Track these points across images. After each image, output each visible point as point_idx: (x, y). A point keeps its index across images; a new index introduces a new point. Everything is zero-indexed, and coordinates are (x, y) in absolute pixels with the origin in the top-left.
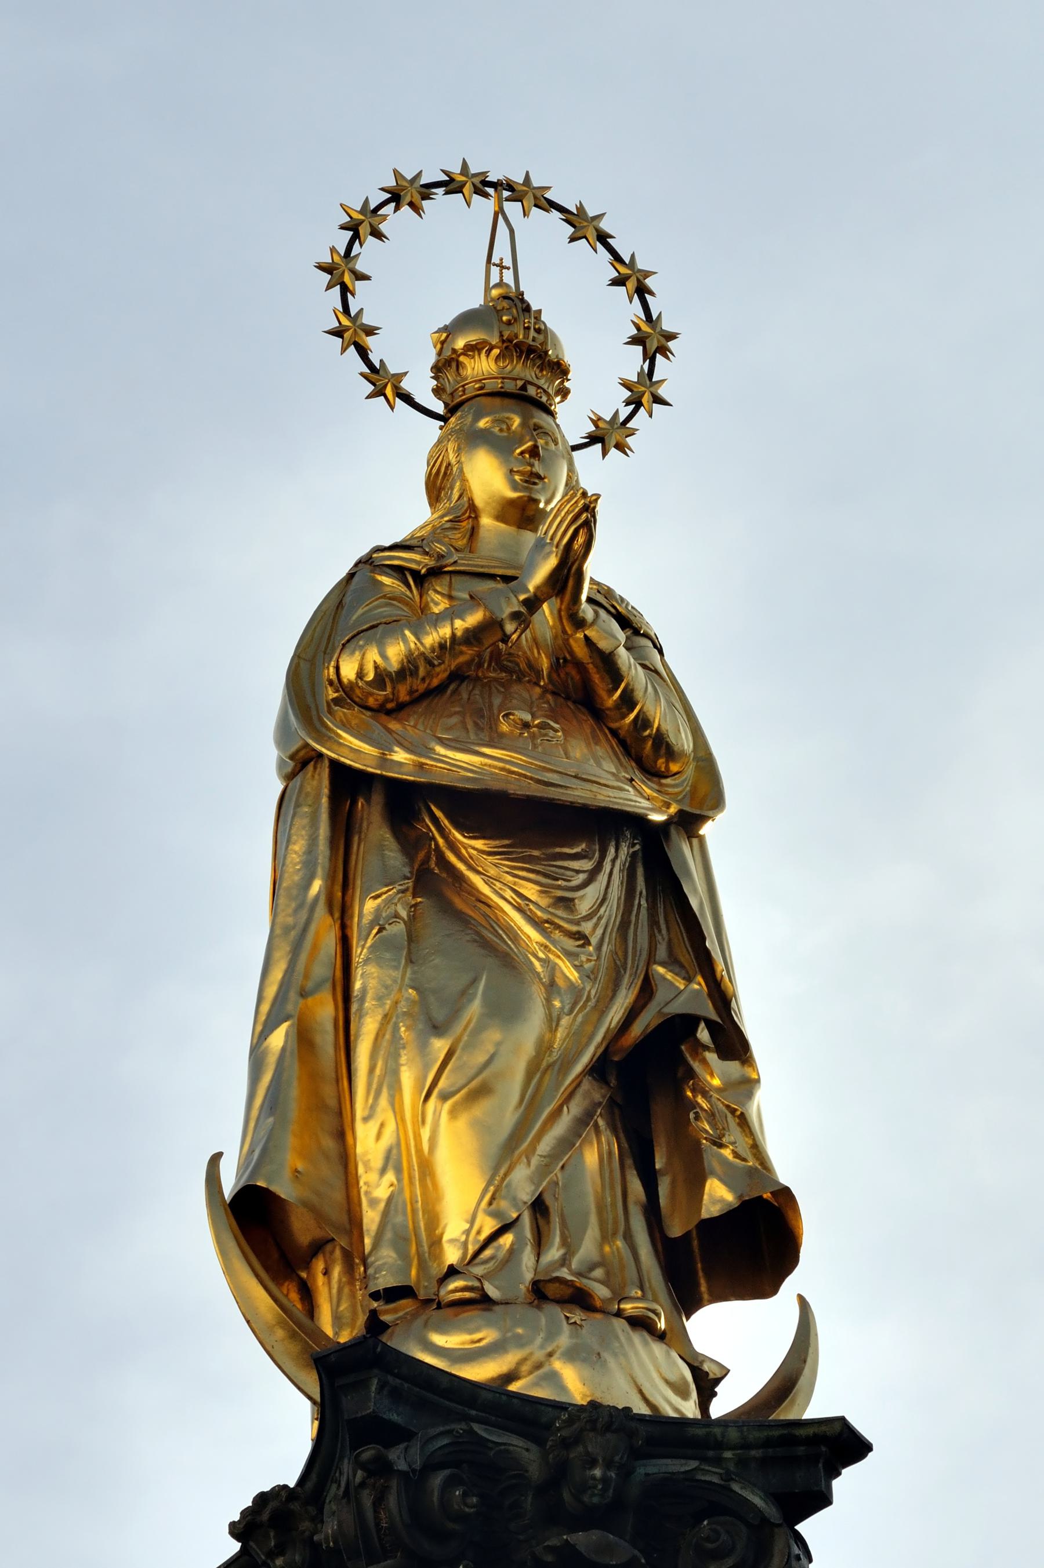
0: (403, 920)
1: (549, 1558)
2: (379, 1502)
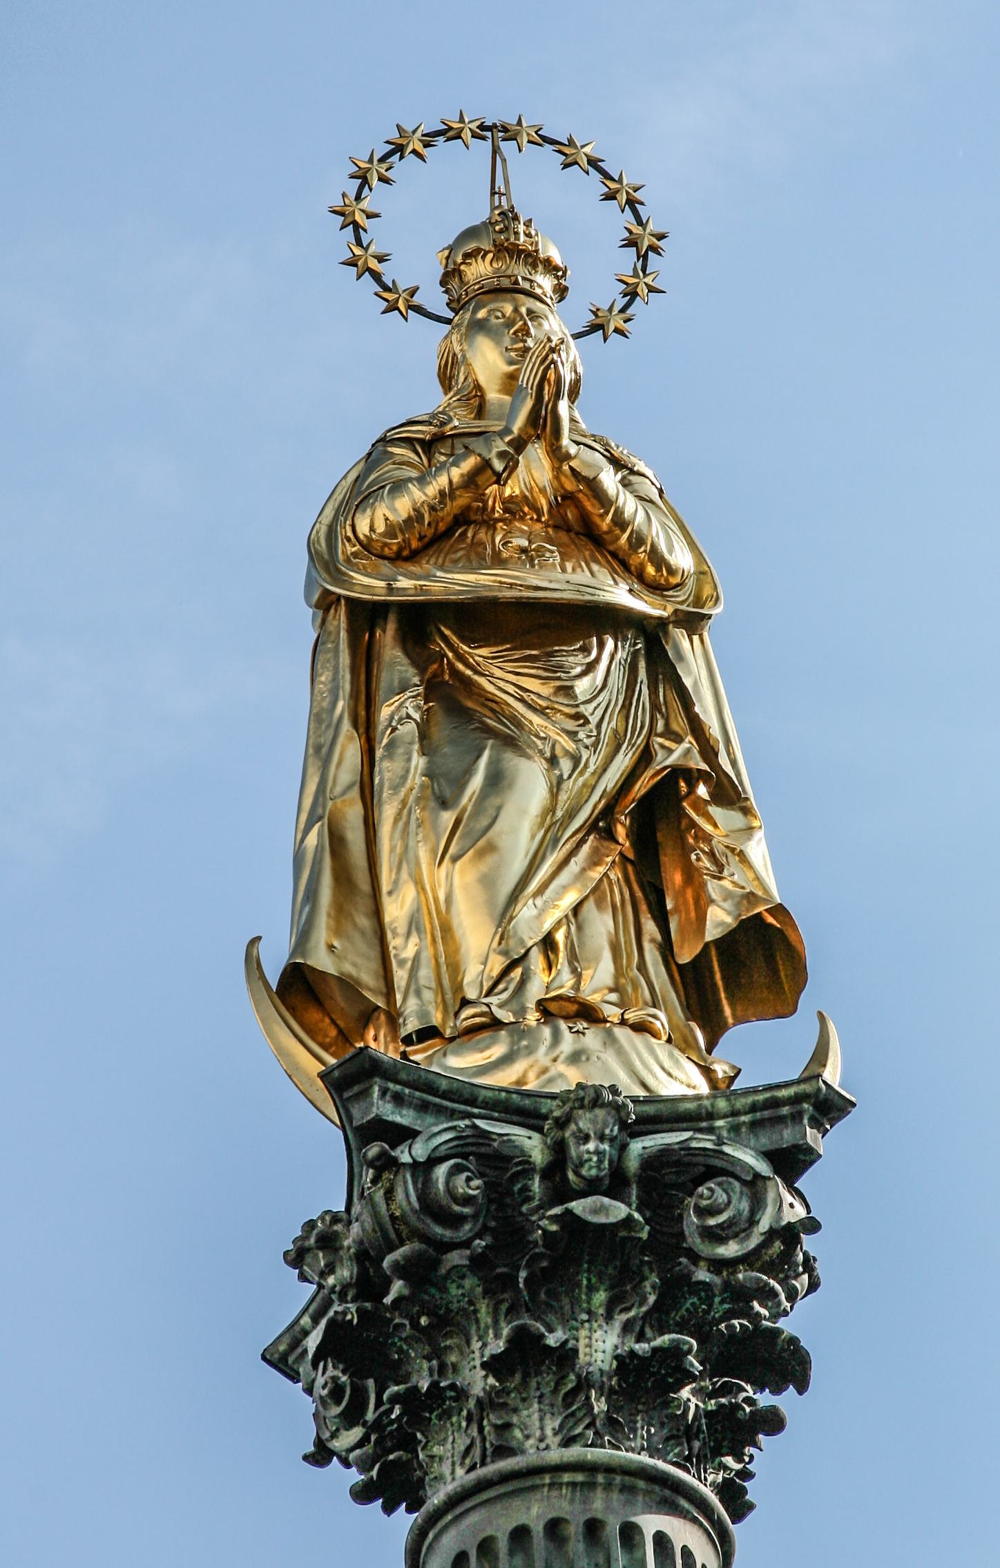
0: (415, 720)
1: (554, 1228)
2: (389, 1194)
